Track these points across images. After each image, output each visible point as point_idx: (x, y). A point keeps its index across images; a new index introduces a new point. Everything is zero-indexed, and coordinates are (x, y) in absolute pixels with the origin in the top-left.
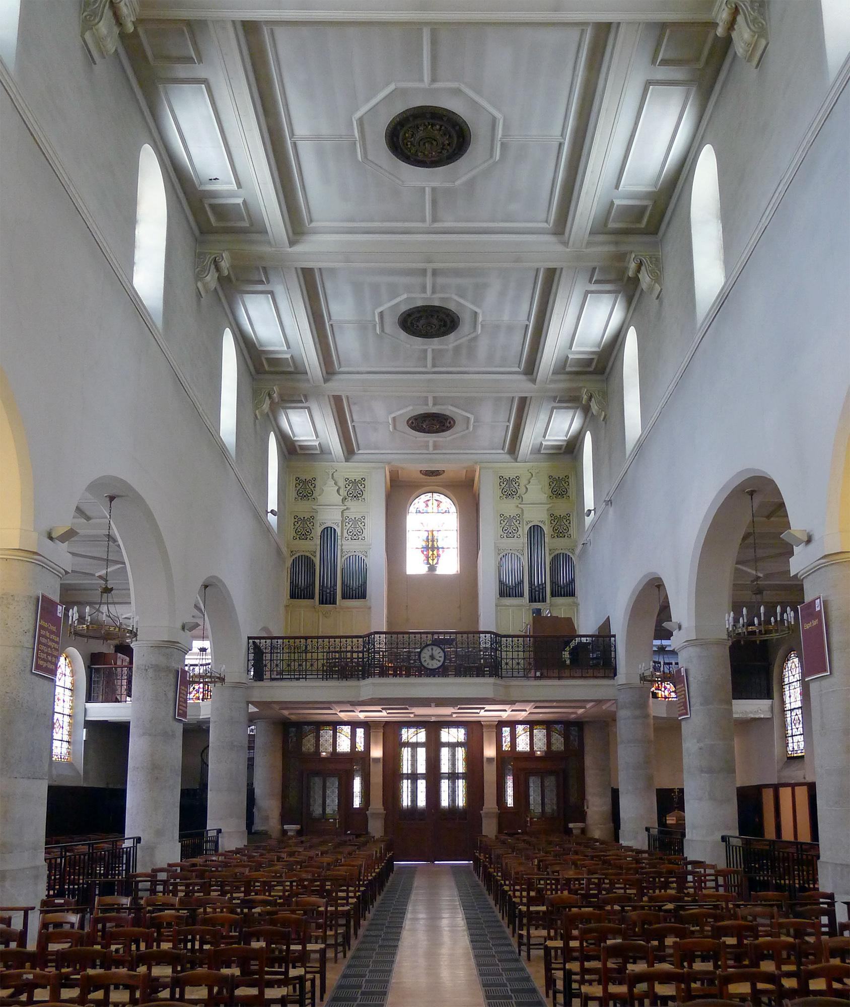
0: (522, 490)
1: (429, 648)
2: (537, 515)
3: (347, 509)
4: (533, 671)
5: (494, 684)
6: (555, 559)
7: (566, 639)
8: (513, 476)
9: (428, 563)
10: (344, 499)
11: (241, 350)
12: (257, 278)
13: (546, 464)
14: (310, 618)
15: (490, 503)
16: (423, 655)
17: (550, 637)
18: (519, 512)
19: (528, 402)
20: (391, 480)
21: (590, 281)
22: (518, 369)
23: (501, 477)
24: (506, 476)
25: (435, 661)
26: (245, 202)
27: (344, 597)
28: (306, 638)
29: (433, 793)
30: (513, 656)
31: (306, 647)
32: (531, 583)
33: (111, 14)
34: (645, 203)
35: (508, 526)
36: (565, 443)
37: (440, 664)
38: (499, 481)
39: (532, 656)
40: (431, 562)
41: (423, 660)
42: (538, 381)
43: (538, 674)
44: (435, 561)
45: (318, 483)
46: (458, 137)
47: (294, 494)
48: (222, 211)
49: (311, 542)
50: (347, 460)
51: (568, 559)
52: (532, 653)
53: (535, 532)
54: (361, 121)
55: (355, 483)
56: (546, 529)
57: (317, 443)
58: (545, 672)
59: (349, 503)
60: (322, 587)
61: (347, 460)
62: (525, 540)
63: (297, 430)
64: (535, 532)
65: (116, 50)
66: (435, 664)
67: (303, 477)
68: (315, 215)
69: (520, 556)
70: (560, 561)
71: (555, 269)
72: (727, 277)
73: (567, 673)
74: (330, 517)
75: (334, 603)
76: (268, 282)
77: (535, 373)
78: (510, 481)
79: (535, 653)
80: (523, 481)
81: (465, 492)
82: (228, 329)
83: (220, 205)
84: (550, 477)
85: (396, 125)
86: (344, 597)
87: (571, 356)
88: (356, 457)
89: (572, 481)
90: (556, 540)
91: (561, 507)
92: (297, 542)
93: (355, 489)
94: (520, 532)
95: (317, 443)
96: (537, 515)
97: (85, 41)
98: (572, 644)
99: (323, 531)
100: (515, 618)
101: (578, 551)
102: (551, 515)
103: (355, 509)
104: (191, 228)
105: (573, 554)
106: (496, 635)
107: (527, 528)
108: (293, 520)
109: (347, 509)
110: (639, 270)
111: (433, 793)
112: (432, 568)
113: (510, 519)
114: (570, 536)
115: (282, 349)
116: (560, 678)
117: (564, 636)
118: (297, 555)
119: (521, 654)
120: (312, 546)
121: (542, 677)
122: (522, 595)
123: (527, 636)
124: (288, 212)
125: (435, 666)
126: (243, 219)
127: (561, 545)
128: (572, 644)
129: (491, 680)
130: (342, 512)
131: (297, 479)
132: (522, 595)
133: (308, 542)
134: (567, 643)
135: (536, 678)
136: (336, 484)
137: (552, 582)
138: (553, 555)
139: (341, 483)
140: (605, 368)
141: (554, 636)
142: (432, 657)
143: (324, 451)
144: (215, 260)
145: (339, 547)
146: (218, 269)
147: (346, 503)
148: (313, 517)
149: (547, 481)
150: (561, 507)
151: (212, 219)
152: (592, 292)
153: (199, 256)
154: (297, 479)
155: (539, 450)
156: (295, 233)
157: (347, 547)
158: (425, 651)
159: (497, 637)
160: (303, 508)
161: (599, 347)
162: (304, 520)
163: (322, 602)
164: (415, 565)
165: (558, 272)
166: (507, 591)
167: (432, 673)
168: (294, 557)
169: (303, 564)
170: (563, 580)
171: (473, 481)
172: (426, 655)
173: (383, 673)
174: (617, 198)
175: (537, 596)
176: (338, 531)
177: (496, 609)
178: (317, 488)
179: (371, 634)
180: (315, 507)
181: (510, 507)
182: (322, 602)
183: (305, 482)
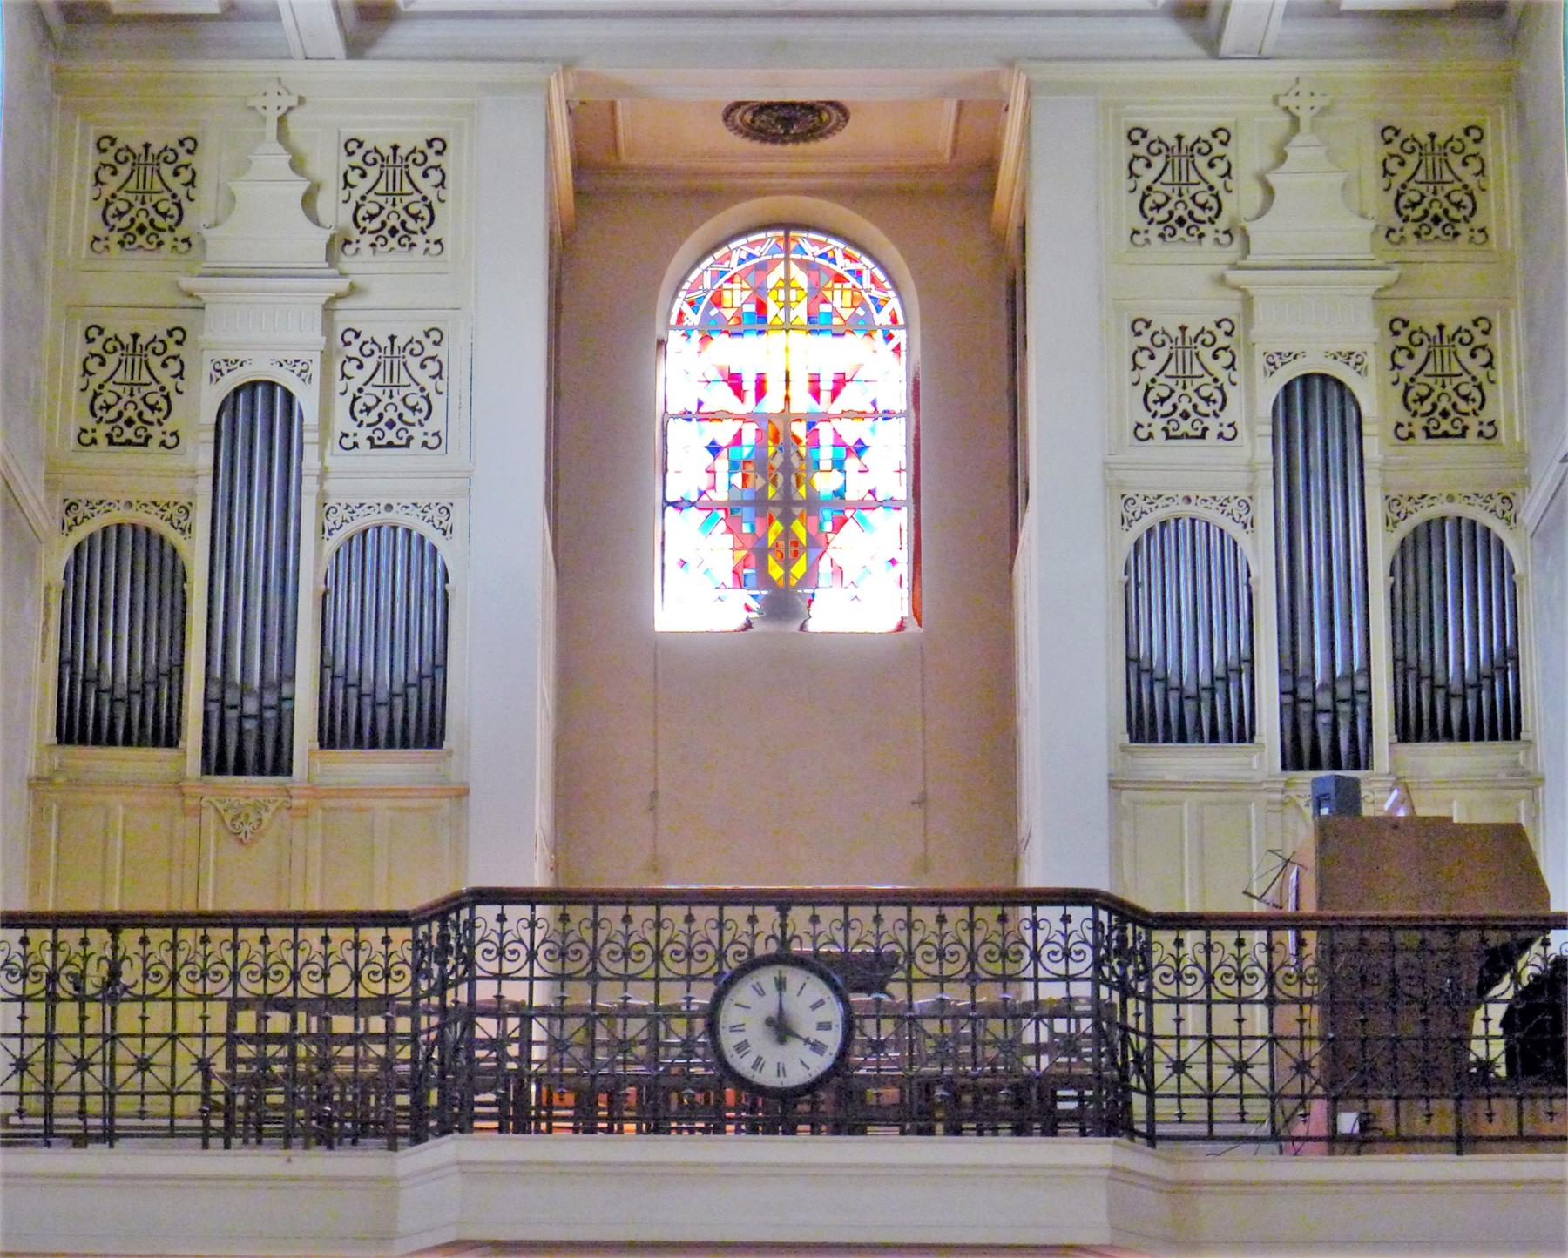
0: (1241, 200)
1: (766, 977)
2: (1326, 322)
3: (353, 290)
4: (1318, 1108)
5: (1117, 1174)
6: (1419, 547)
7: (1495, 939)
8: (1196, 127)
9: (764, 579)
10: (338, 245)
13: (1360, 70)
14: (152, 828)
15: (1084, 274)
16: (730, 1015)
17: (1415, 924)
18: (1230, 307)
20: (580, 167)
23: (1136, 135)
24: (1163, 127)
25: (796, 1049)
27: (328, 738)
28: (114, 923)
29: (1310, 1001)
30: (1223, 1026)
31: (114, 973)
32: (1291, 670)
35: (1175, 382)
37: (820, 1064)
38: (1127, 151)
39: (1314, 1029)
40: (776, 572)
41: (728, 1041)
43: (1348, 1122)
44: (799, 569)
45: (206, 163)
47: (90, 222)
49: (170, 461)
50: (356, 48)
51: (1481, 546)
52: (1313, 1013)
53: (1312, 402)
55: (394, 162)
56: (1374, 396)
58: (1383, 1108)
59: (363, 263)
60: (216, 701)
61: (356, 48)
62: (1256, 448)
64: (1312, 402)
66: (797, 1066)
67: (132, 135)
69: (1233, 530)
70: (1454, 559)
73: (1503, 1115)
74: (262, 331)
75: (281, 765)
78: (1182, 154)
79: (1332, 1006)
80: (1248, 156)
81: (955, 227)
84: (1388, 133)
86: (328, 738)
89: (1499, 152)
90: (1423, 449)
91: (1446, 285)
92: (102, 457)
93: (394, 195)
94: (1233, 412)
96: (1326, 322)
98: (1530, 965)
99: (229, 404)
100: (1231, 835)
101: (1531, 509)
102: (1396, 325)
103: (393, 293)
105: (1511, 520)
106: (1124, 912)
107: (1269, 390)
108: (80, 350)
109: (353, 290)
111: (1310, 1001)
112: (783, 604)
113: (1186, 341)
114: (1490, 434)
116: (1462, 1142)
117: (1482, 924)
118: (94, 525)
119: (1257, 1020)
120: (174, 479)
121: (1365, 1140)
122: (1244, 733)
123: (1298, 923)
125: (797, 1076)
127: (1444, 477)
128: (1530, 965)
129: (1100, 1151)
130: (329, 308)
131: (105, 142)
132: (1244, 733)
133: (150, 459)
134: (1500, 961)
135: (1334, 1141)
136: (297, 165)
137: (1402, 666)
138: (1405, 528)
139: (327, 164)
141: (1432, 925)
142: (781, 1028)
145: (310, 485)
147: (347, 262)
148: (178, 334)
149: (1371, 153)
150: (1446, 285)
154: (105, 142)
157: (347, 481)
158: (743, 992)
159: (1126, 930)
160: (131, 288)
162: (135, 349)
163: (217, 762)
164: (695, 588)
166: (1162, 712)
167: (776, 1111)
168: (81, 533)
169: (122, 569)
170: (1456, 655)
171: (990, 166)
172: (746, 1012)
173: (518, 1117)
175: (1322, 743)
176: (307, 400)
177: (1116, 815)
178: (206, 190)
179: (457, 902)
180: (187, 282)
181: (1182, 282)
182: (217, 762)
183: (144, 160)
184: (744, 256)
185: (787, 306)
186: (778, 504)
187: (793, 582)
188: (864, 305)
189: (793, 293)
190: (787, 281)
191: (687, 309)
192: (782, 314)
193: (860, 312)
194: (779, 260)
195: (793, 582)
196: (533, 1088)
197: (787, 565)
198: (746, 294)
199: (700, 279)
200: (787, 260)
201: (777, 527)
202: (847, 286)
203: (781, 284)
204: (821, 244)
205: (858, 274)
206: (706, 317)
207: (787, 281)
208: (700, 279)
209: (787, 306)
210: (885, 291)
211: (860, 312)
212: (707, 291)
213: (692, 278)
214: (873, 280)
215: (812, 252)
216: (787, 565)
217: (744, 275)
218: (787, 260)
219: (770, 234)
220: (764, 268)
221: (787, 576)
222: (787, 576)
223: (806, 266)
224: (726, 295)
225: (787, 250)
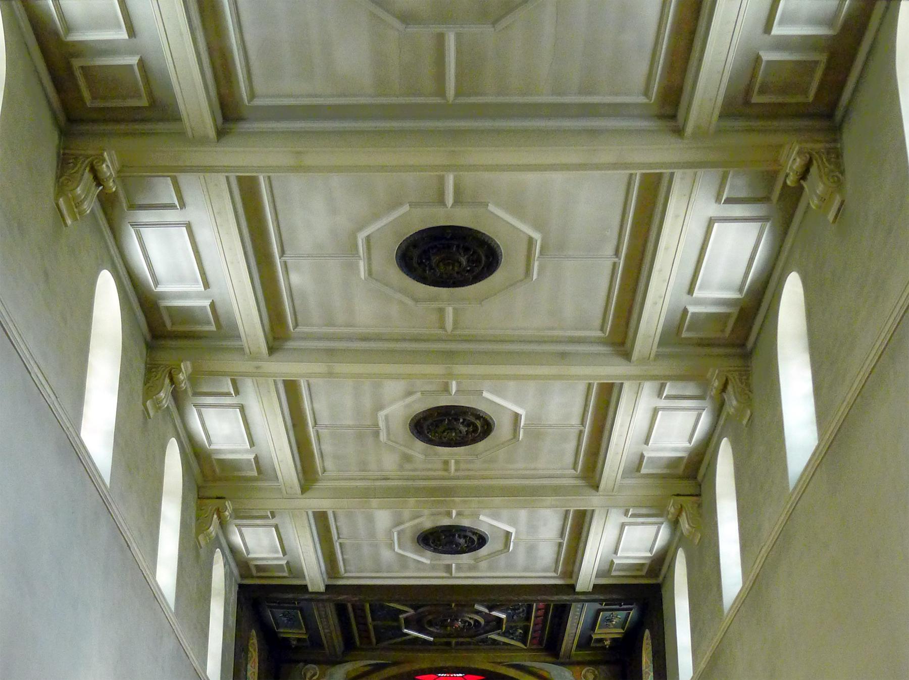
11: (131, 309)
12: (225, 390)
19: (587, 519)
21: (660, 395)
22: (555, 575)
26: (142, 63)
33: (92, 177)
34: (815, 56)
36: (734, 311)
42: (602, 486)
46: (487, 257)
48: (107, 81)
54: (368, 239)
57: (284, 562)
63: (160, 269)
65: (92, 211)
68: (259, 88)
71: (660, 176)
72: (744, 583)
76: (183, 205)
77: (574, 577)
82: (218, 550)
83: (99, 66)
85: (407, 248)
87: (692, 309)
88: (290, 344)
95: (284, 562)
97: (57, 205)
104: (20, 27)
110: (804, 174)
115: (206, 328)
124: (298, 448)
126: (209, 323)
140: (834, 105)
143: (262, 469)
144: (170, 373)
146: (98, 180)
151: (86, 94)
152: (664, 409)
153: (65, 163)
155: (609, 571)
156: (226, 119)
161: (651, 551)
165: (588, 515)
174: (690, 304)
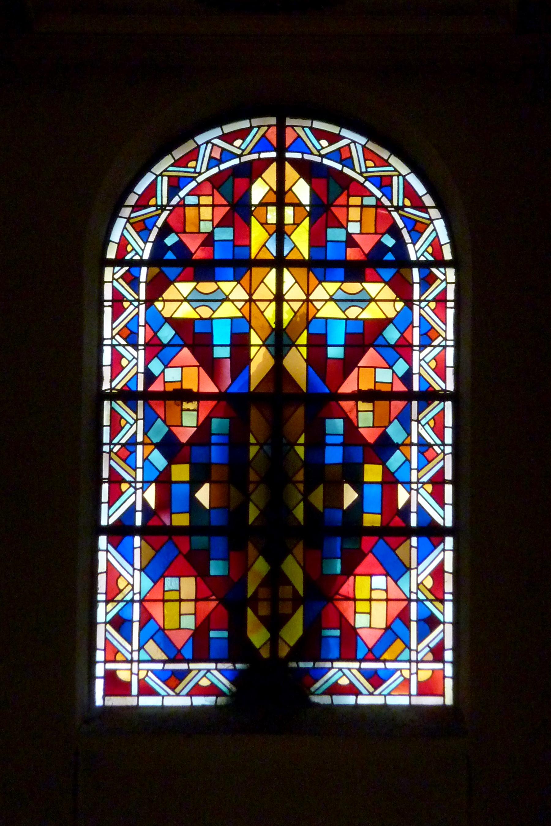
40: (258, 636)
44: (294, 630)
184: (217, 154)
185: (280, 232)
186: (275, 486)
187: (284, 652)
188: (394, 231)
189: (289, 212)
190: (281, 197)
191: (133, 237)
192: (272, 246)
193: (389, 241)
194: (269, 161)
195: (284, 652)
196: (253, 513)
197: (275, 624)
198: (222, 212)
199: (152, 190)
200: (281, 161)
201: (261, 566)
202: (370, 201)
203: (287, 229)
204: (333, 138)
205: (384, 183)
206: (159, 247)
207: (281, 197)
208: (152, 190)
209: (280, 232)
210: (424, 208)
211: (389, 241)
212: (163, 208)
213: (140, 188)
214: (409, 191)
215: (320, 151)
216: (275, 624)
217: (216, 182)
218: (281, 161)
219: (256, 122)
220: (250, 171)
221: (274, 641)
222: (274, 641)
223: (307, 170)
224: (190, 213)
225: (281, 148)
